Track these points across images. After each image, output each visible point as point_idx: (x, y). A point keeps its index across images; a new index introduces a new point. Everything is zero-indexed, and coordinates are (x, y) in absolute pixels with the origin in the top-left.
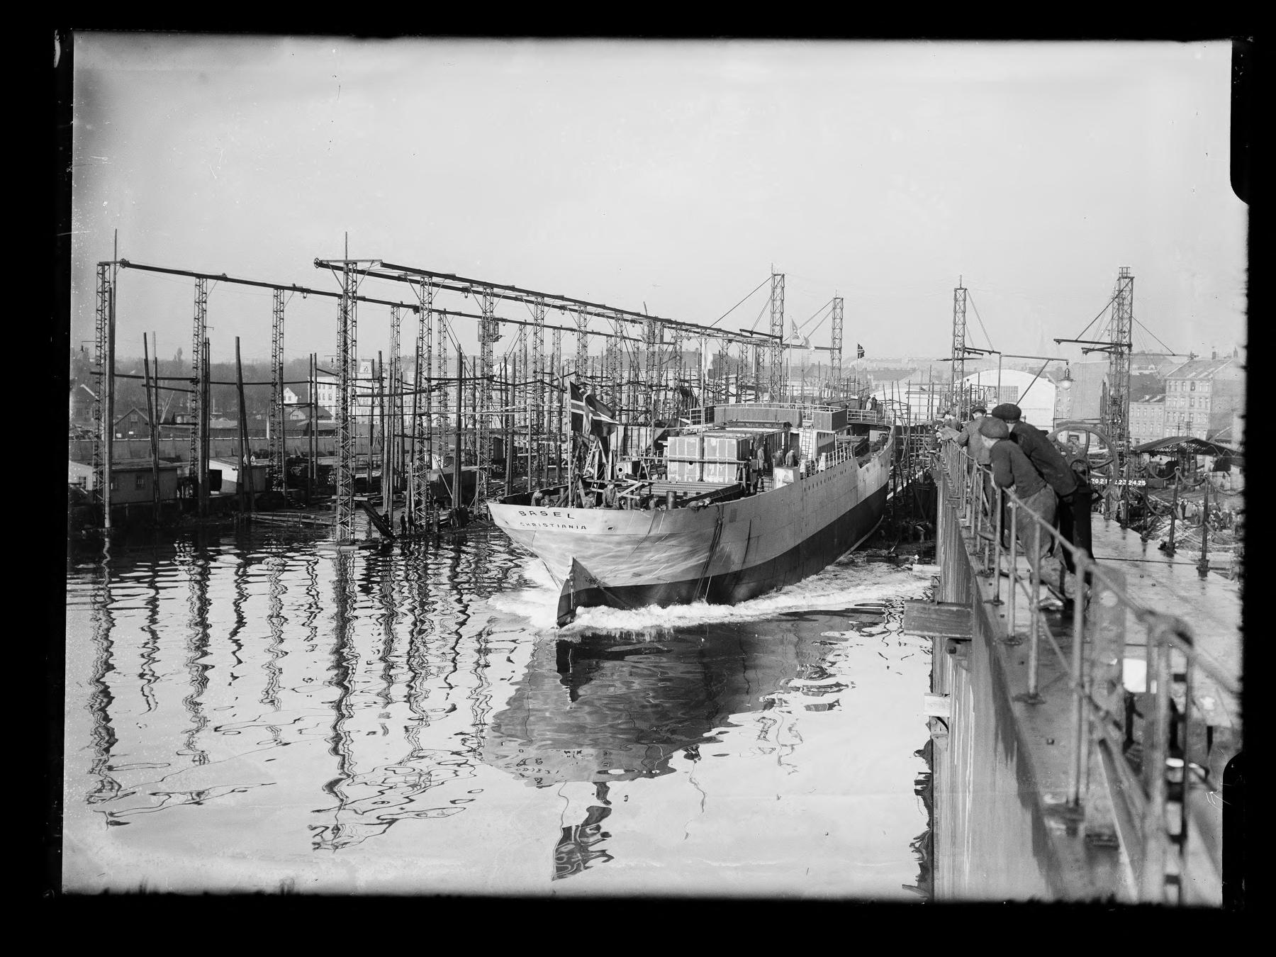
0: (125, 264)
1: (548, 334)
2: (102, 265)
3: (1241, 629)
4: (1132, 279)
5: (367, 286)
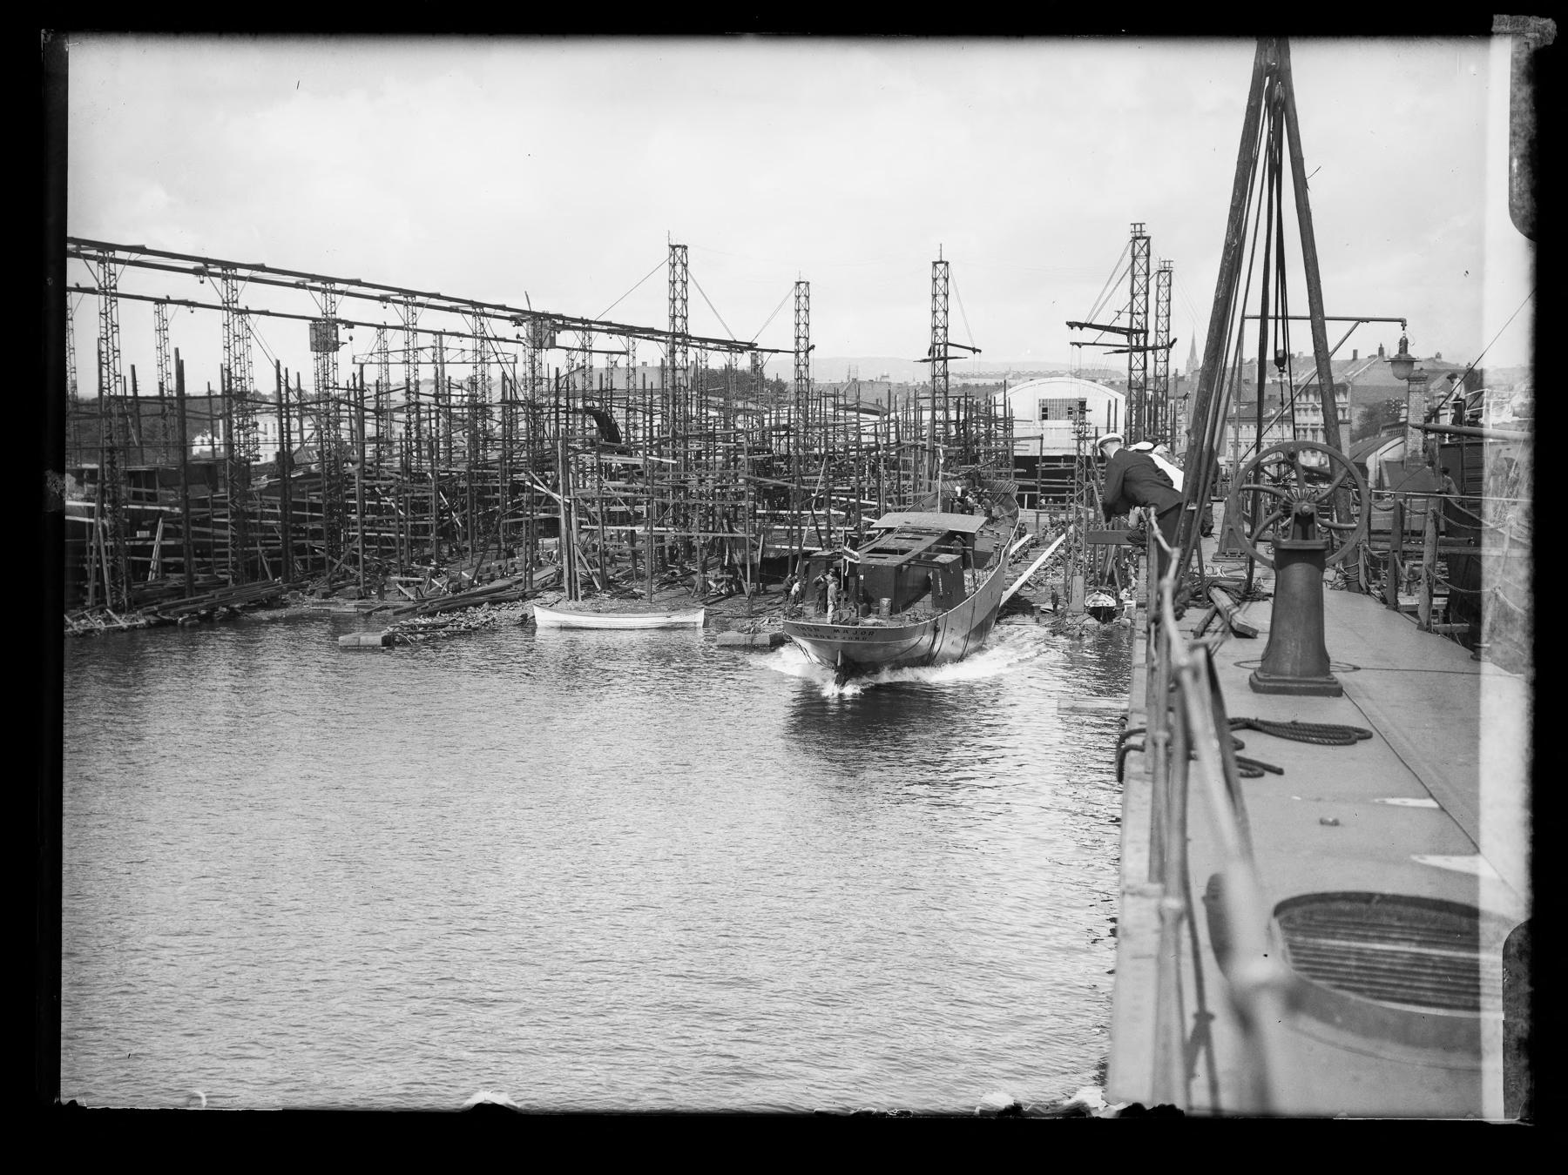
4: (1148, 239)
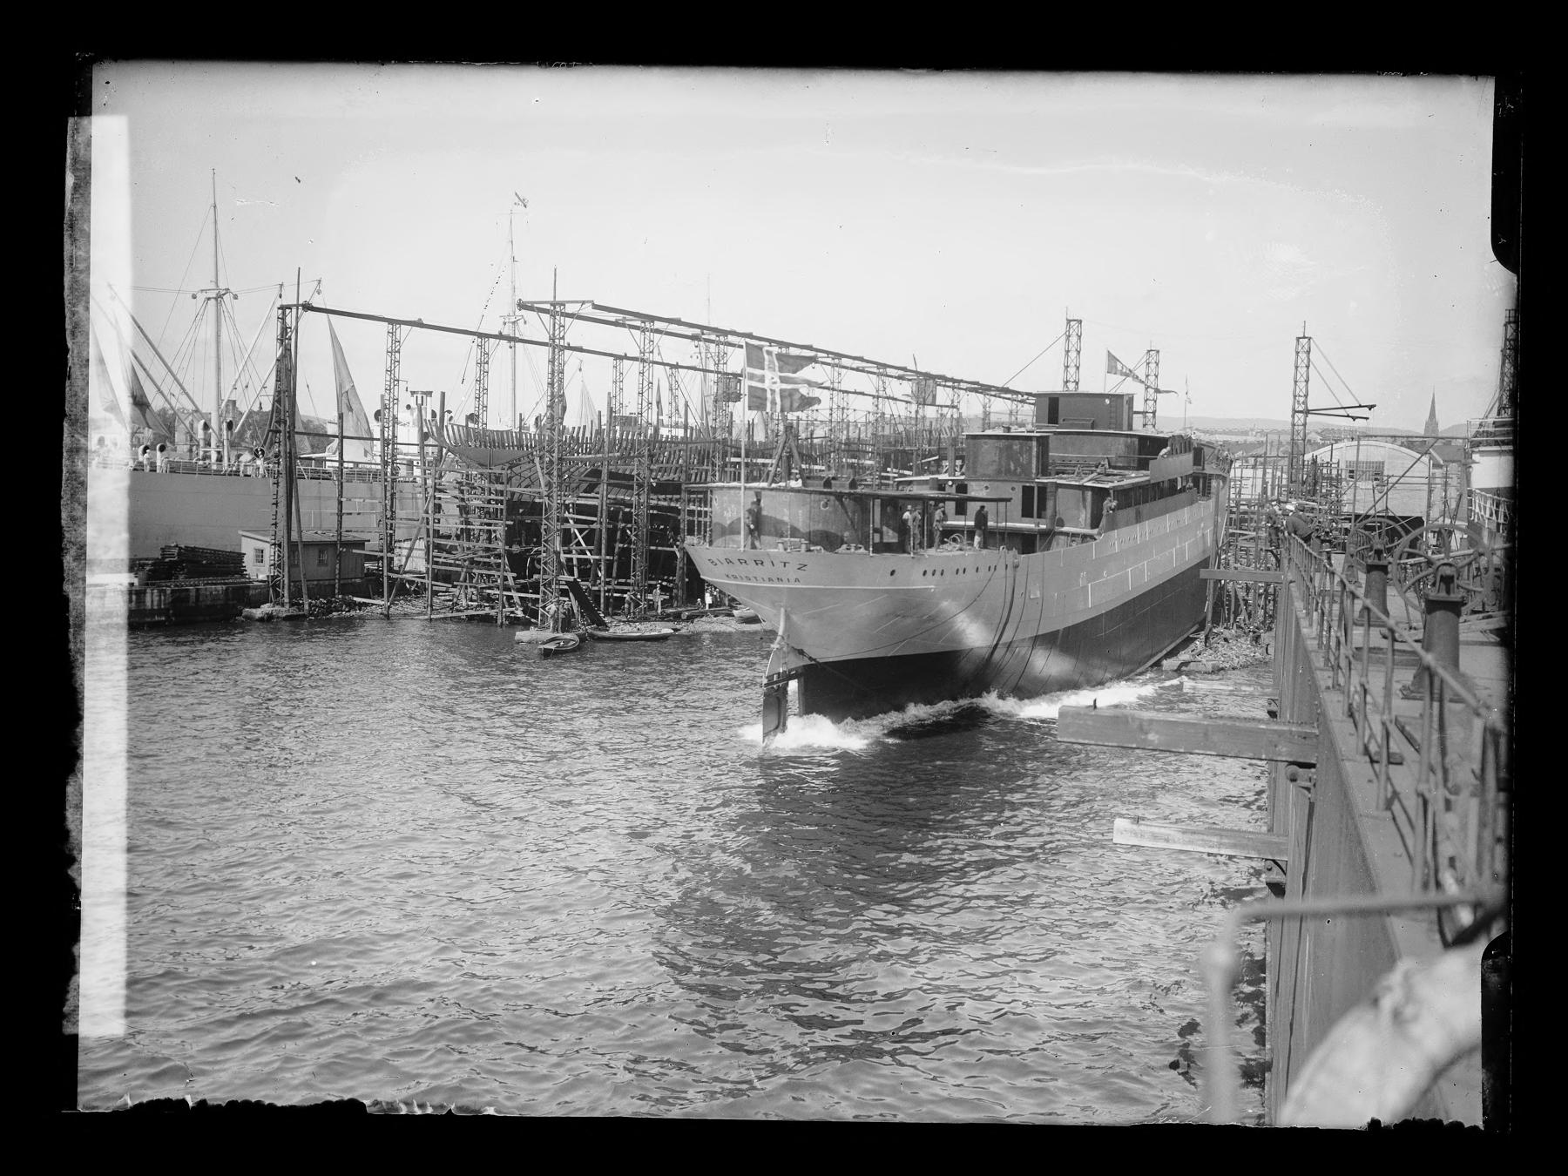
0: (308, 307)
1: (659, 373)
2: (283, 308)
3: (1375, 1123)
5: (576, 333)
